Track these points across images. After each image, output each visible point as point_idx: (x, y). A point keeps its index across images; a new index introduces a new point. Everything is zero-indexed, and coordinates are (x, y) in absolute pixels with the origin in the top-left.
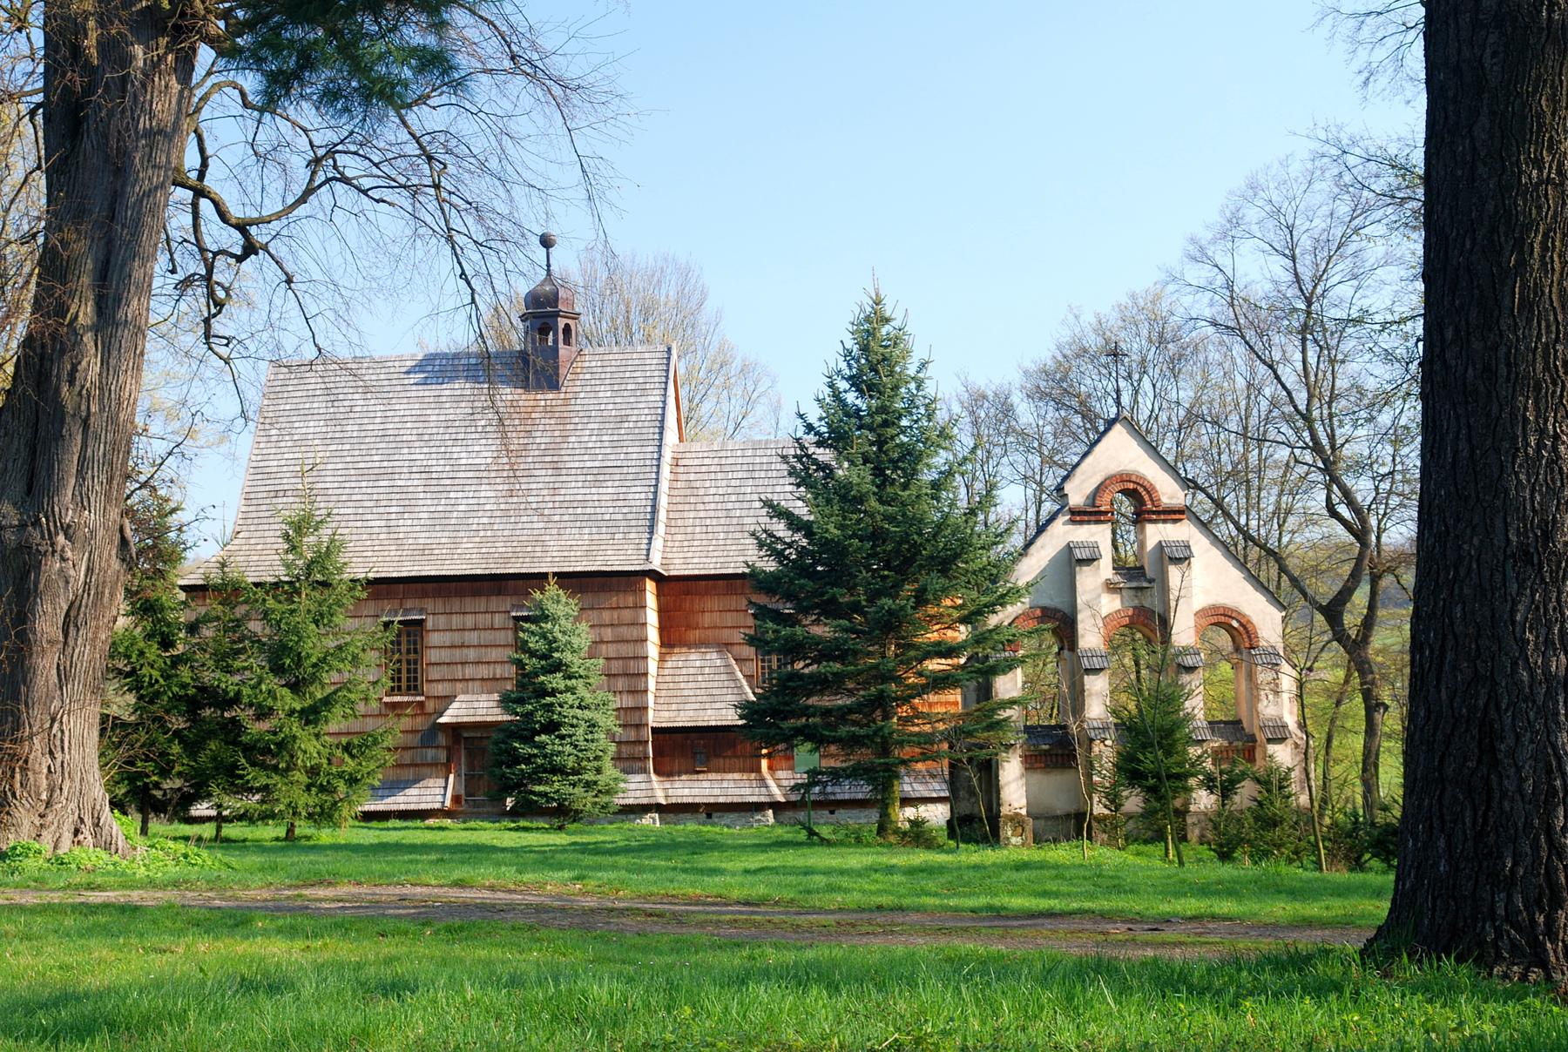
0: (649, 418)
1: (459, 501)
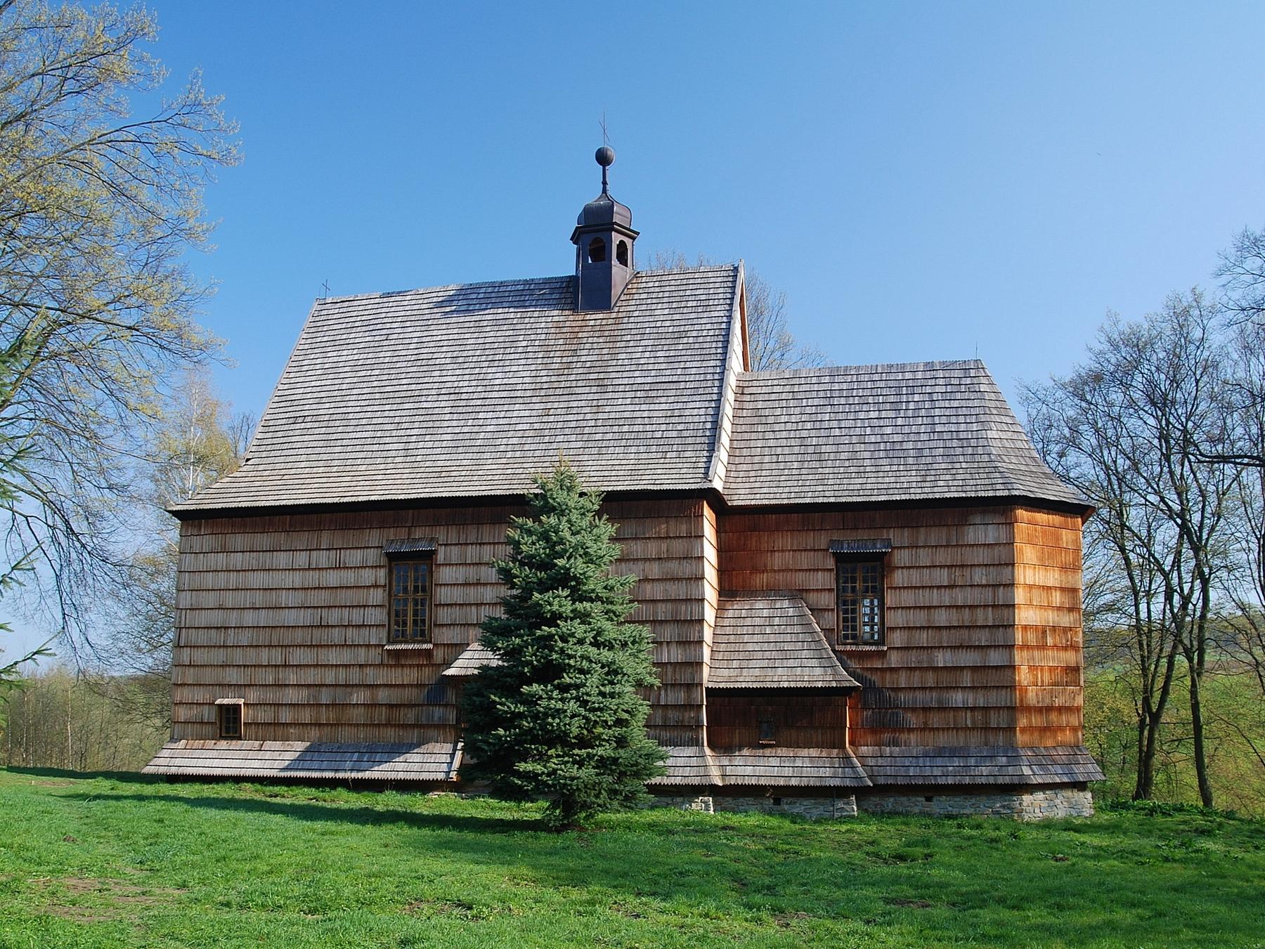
0: (711, 333)
1: (488, 422)
